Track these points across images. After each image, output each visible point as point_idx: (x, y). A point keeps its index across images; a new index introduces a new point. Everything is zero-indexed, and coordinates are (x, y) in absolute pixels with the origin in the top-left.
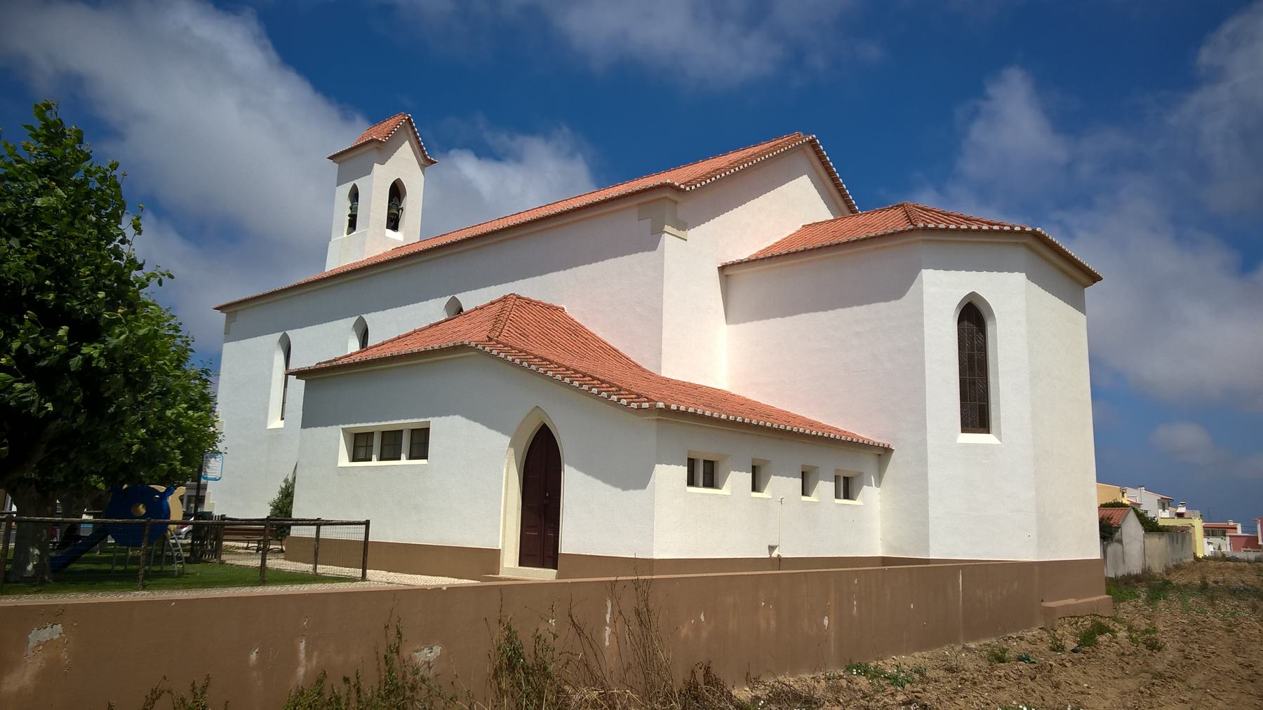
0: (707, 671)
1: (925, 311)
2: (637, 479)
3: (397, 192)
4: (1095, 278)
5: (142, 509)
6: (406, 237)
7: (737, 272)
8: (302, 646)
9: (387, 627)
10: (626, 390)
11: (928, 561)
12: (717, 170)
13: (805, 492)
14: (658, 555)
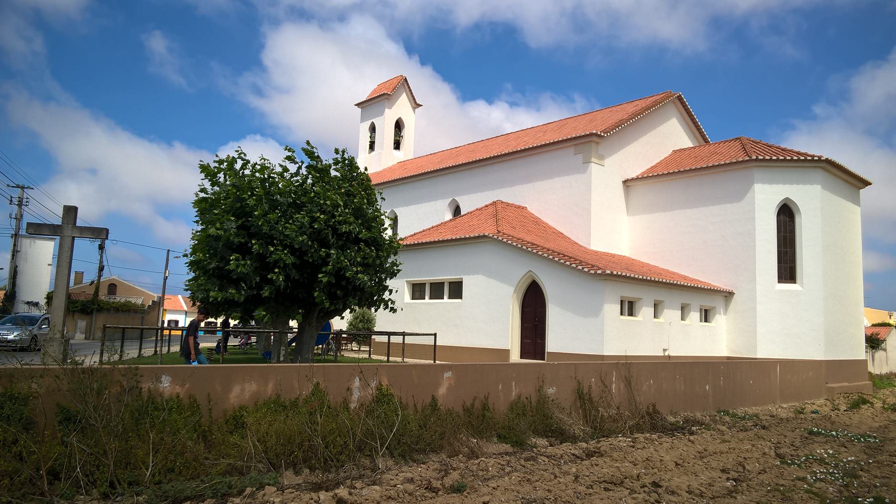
0: (654, 406)
1: (756, 210)
2: (596, 312)
3: (399, 126)
4: (866, 183)
5: (253, 323)
6: (407, 153)
7: (634, 184)
8: (514, 383)
9: (538, 378)
10: (585, 262)
11: (756, 359)
12: (621, 120)
13: (683, 319)
14: (605, 354)
